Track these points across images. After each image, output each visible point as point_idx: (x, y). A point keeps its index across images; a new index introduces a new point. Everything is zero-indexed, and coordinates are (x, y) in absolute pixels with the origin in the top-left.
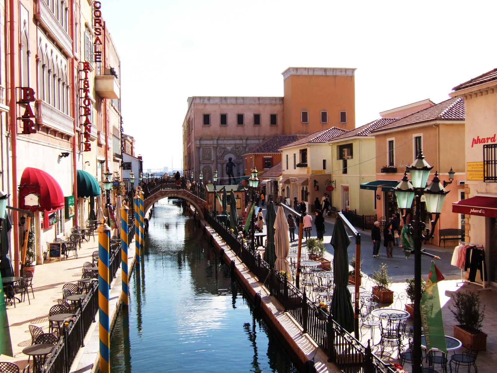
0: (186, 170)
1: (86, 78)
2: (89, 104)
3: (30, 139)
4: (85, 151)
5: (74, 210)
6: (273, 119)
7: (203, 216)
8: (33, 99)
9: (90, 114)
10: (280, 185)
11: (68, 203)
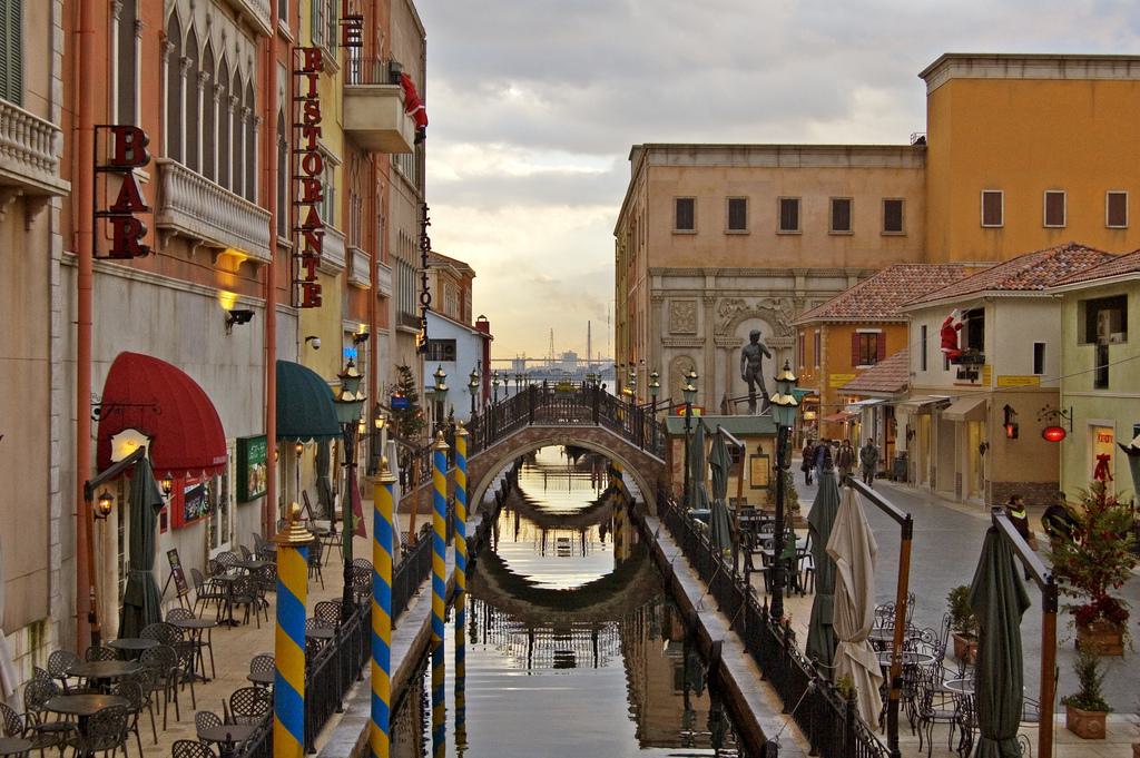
0: (623, 366)
1: (313, 93)
2: (319, 170)
3: (133, 271)
4: (304, 306)
5: (264, 477)
6: (893, 214)
7: (653, 507)
8: (142, 161)
9: (321, 199)
10: (902, 420)
11: (246, 457)
